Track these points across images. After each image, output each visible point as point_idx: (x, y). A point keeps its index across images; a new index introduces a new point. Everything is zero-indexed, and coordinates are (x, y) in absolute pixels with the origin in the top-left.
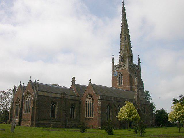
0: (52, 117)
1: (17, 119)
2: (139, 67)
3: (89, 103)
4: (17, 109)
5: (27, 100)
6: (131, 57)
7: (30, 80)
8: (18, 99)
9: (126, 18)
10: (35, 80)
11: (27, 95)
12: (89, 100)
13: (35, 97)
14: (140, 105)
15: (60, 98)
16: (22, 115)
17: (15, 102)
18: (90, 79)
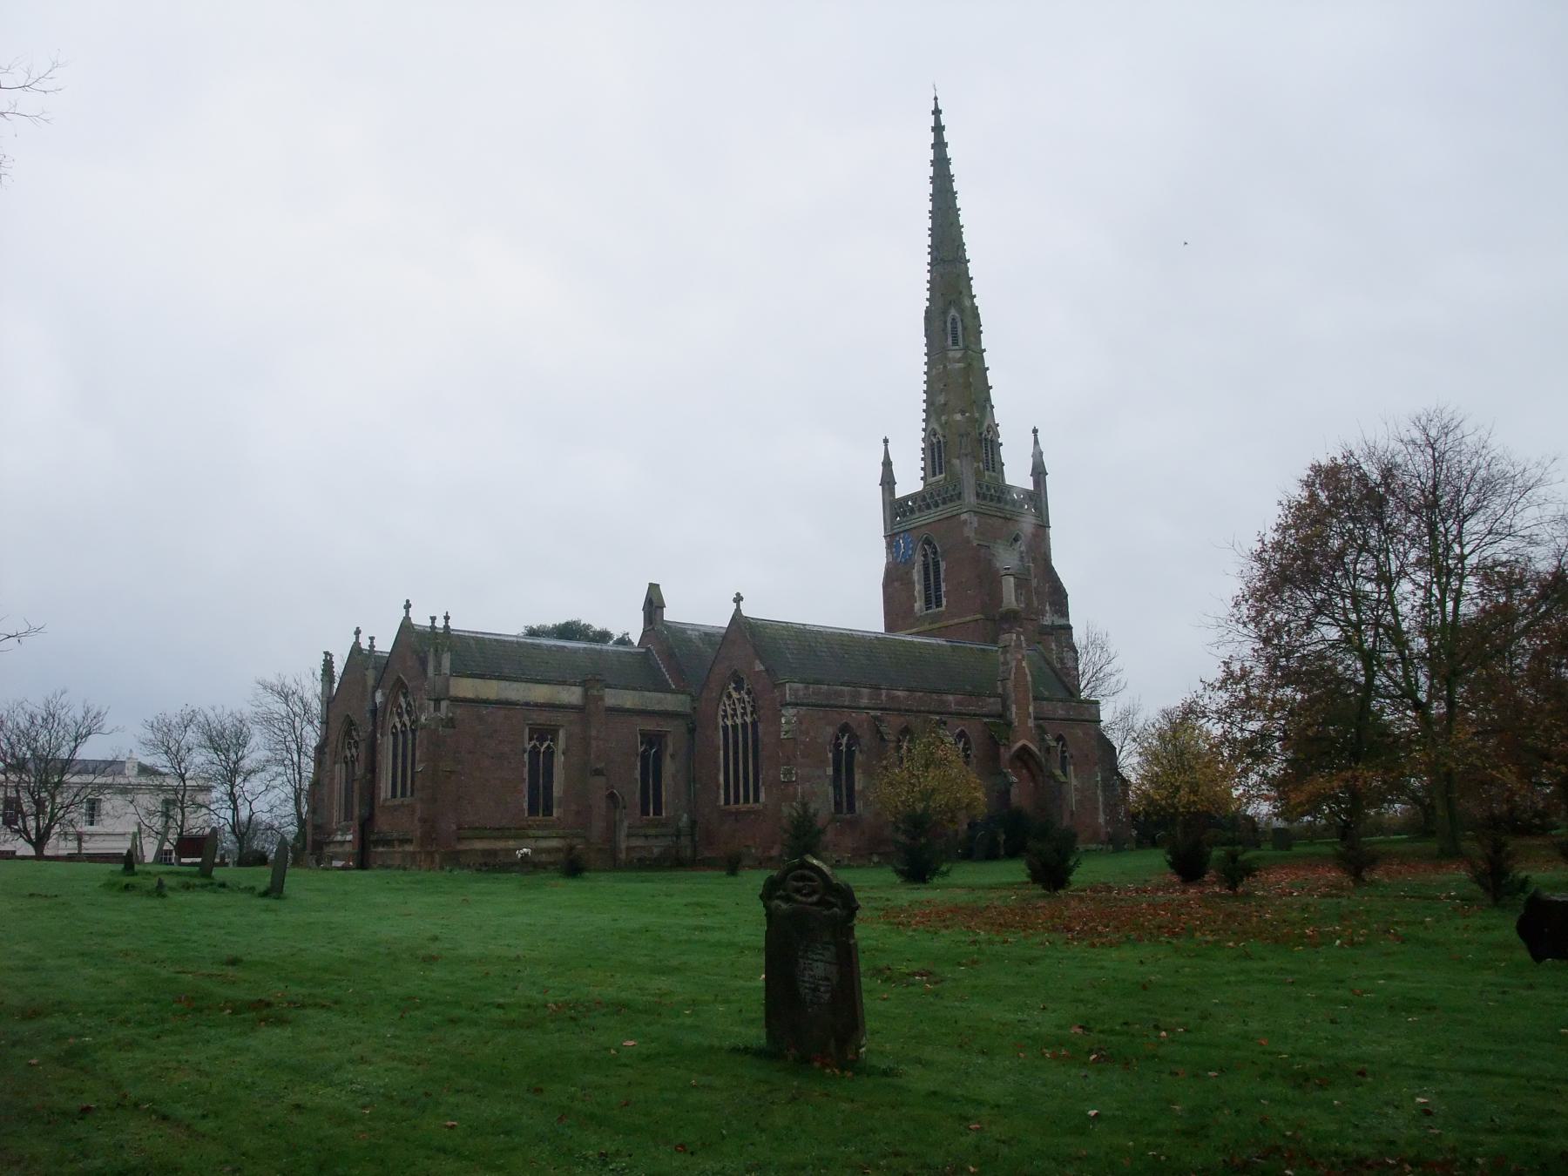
0: (533, 810)
1: (349, 837)
2: (1037, 498)
3: (735, 727)
4: (350, 780)
5: (395, 727)
6: (986, 446)
7: (407, 618)
8: (351, 723)
9: (955, 212)
10: (433, 619)
11: (396, 698)
12: (735, 710)
13: (437, 708)
14: (1031, 723)
15: (573, 707)
16: (377, 811)
17: (333, 738)
18: (738, 594)
